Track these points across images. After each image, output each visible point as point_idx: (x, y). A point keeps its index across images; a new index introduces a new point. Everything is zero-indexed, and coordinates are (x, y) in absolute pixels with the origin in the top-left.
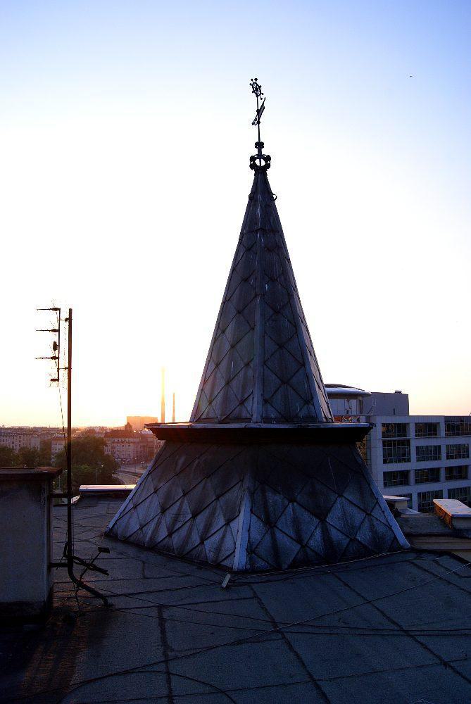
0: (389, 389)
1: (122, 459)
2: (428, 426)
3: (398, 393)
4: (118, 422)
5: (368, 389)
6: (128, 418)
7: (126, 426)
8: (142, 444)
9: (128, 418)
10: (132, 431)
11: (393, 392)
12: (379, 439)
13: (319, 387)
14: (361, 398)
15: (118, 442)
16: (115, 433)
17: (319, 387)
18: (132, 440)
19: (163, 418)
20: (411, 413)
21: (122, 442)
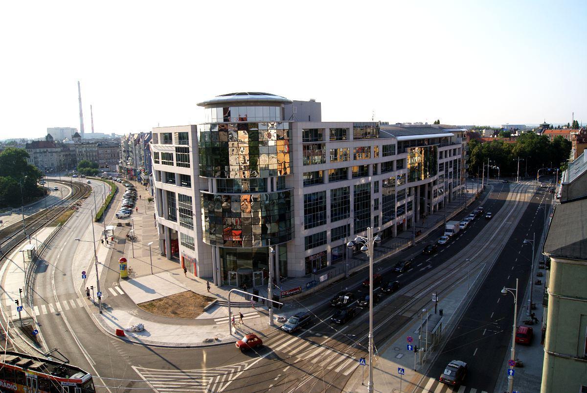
0: (307, 99)
1: (46, 168)
2: (340, 133)
3: (313, 101)
4: (40, 135)
5: (291, 98)
6: (48, 129)
7: (47, 137)
8: (64, 153)
9: (48, 129)
10: (52, 142)
11: (308, 100)
12: (300, 143)
13: (69, 235)
14: (283, 106)
15: (40, 153)
16: (35, 144)
17: (69, 235)
18: (54, 150)
19: (82, 129)
20: (323, 120)
21: (45, 152)
